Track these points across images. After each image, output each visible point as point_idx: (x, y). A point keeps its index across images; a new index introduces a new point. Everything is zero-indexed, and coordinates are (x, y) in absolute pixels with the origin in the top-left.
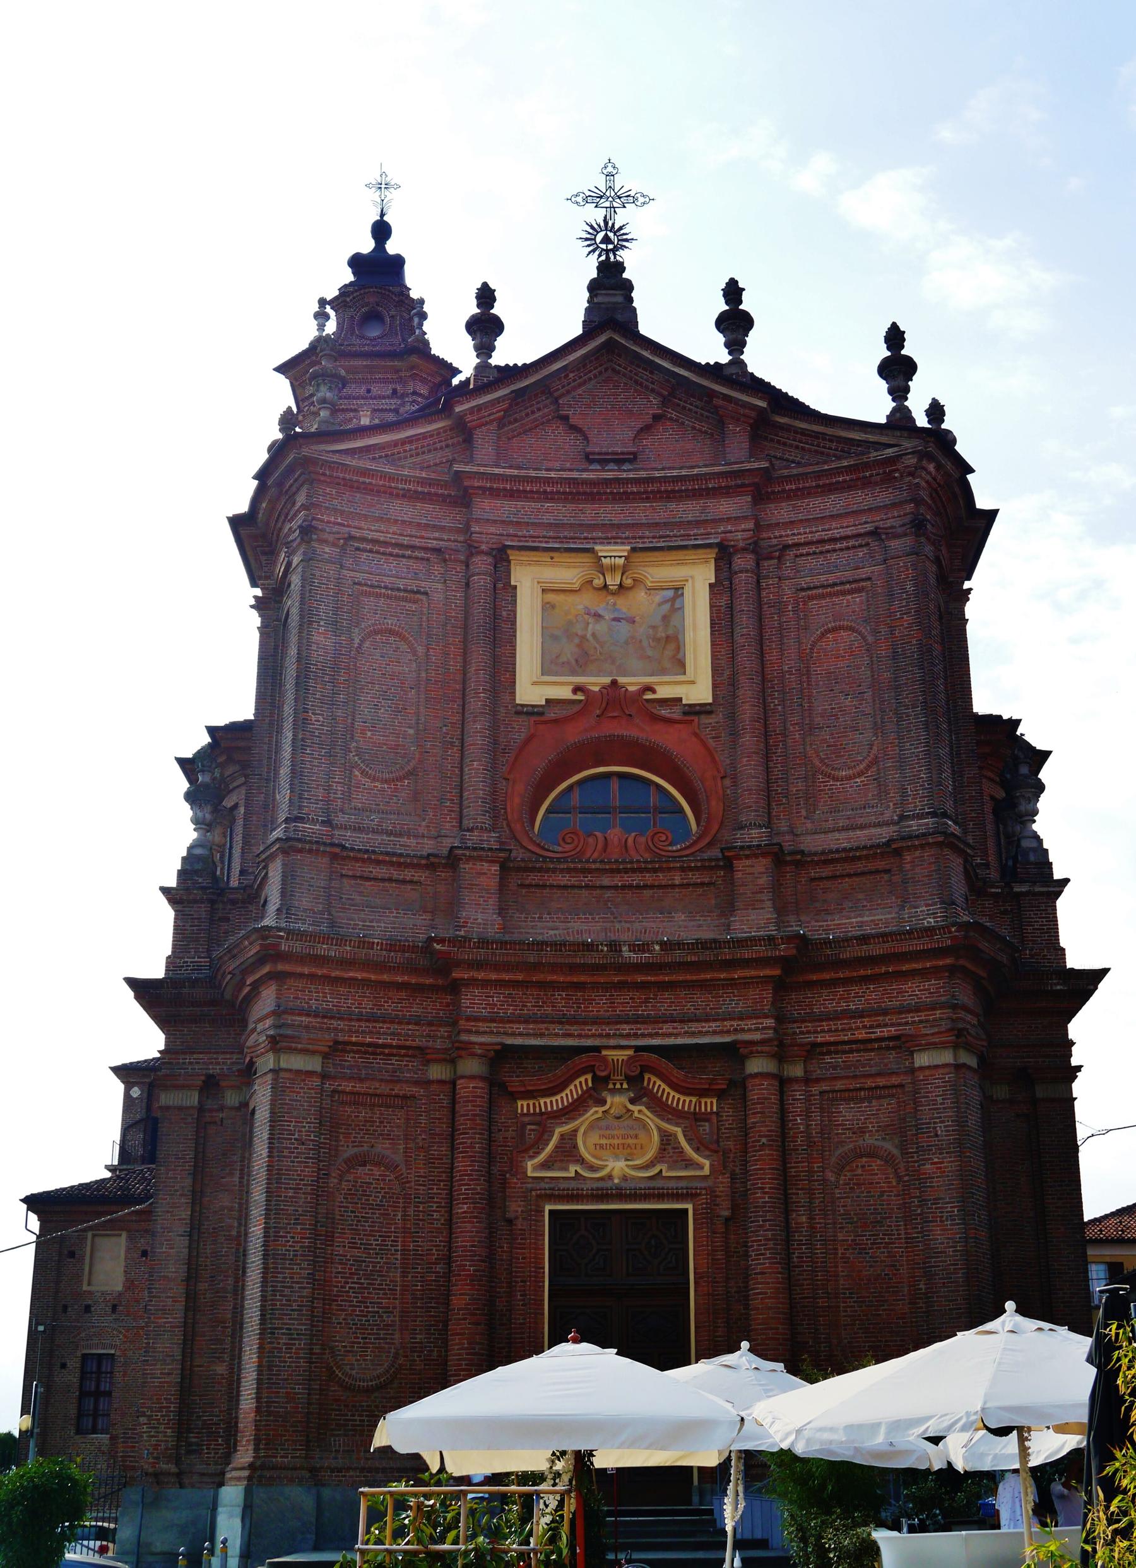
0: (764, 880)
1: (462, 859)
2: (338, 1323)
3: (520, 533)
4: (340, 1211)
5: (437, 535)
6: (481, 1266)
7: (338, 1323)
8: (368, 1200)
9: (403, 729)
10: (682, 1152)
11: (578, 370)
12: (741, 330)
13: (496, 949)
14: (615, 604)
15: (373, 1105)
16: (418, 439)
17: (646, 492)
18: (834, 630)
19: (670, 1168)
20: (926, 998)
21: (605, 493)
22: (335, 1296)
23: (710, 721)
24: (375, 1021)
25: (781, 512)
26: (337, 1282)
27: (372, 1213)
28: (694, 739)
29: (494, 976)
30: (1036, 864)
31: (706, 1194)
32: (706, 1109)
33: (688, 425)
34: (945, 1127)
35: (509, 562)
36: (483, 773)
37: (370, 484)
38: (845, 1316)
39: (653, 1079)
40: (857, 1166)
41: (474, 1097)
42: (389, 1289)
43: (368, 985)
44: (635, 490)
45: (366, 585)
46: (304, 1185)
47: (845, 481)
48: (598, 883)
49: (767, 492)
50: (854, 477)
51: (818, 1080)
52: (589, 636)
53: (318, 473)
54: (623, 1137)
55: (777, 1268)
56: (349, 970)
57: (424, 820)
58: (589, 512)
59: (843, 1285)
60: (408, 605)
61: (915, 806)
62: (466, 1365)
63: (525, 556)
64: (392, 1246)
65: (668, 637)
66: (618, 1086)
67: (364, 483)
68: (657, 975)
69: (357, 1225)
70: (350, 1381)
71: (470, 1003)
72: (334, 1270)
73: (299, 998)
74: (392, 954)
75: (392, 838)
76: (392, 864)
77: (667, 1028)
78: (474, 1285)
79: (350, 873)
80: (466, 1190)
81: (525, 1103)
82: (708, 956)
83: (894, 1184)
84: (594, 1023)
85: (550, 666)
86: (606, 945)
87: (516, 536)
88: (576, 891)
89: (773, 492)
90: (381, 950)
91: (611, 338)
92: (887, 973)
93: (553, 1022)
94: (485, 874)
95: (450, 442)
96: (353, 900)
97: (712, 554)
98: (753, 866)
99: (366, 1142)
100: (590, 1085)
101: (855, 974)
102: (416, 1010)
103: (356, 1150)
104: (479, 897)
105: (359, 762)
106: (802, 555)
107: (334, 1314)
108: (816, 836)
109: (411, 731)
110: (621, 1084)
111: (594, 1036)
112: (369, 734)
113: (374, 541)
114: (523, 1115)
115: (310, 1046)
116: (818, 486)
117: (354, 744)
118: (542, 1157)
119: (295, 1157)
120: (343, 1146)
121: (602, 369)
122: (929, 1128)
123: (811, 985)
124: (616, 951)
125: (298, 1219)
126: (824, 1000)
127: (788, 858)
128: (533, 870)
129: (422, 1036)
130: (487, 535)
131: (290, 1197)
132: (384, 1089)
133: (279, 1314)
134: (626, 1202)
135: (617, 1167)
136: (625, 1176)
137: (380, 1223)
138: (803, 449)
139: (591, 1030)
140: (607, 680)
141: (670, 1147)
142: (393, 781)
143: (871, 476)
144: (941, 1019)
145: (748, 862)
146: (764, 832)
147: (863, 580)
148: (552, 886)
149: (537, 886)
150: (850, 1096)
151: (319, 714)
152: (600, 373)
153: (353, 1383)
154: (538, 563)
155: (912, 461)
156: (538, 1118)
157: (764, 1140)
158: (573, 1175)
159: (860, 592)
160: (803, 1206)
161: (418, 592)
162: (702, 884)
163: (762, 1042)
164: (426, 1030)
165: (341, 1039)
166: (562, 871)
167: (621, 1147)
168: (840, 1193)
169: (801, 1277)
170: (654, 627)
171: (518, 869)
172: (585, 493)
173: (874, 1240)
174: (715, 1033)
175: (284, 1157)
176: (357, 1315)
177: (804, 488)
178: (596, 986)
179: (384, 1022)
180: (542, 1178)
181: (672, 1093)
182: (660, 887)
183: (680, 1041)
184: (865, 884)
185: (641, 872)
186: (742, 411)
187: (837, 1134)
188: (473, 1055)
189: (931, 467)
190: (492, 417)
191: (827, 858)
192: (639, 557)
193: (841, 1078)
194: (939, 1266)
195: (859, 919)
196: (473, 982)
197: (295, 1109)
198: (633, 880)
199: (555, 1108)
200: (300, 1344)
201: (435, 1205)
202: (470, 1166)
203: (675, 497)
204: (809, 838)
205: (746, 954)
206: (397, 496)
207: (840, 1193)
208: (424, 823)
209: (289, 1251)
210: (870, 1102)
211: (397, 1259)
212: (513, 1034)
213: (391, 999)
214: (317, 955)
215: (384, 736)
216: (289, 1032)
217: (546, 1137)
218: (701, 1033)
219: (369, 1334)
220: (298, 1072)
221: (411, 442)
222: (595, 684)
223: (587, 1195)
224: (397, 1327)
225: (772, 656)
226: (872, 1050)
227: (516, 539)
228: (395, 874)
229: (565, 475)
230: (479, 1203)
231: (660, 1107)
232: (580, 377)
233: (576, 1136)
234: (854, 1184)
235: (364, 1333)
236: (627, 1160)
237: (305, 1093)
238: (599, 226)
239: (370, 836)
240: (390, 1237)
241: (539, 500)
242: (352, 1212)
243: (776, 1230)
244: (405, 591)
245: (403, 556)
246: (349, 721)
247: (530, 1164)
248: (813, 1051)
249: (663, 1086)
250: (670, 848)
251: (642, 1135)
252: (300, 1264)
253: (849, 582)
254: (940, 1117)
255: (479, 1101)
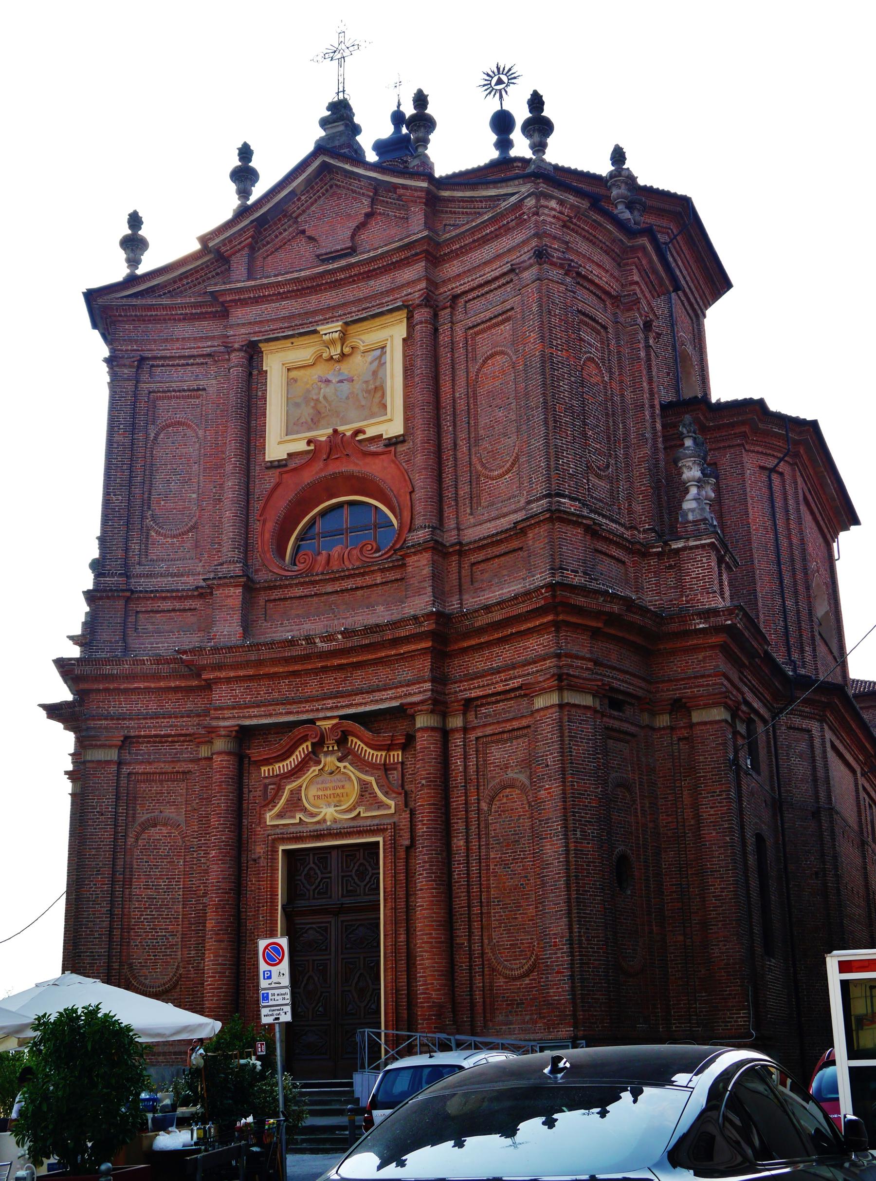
0: (427, 571)
1: (213, 588)
2: (135, 946)
3: (263, 330)
4: (137, 862)
5: (209, 343)
6: (225, 897)
7: (135, 946)
8: (158, 852)
9: (188, 495)
10: (376, 796)
11: (308, 192)
12: (422, 129)
13: (226, 653)
14: (340, 369)
15: (161, 781)
16: (192, 274)
17: (351, 277)
18: (492, 356)
19: (366, 810)
20: (541, 651)
21: (322, 284)
22: (133, 925)
23: (404, 448)
24: (157, 718)
25: (453, 268)
26: (134, 915)
27: (161, 862)
28: (393, 465)
29: (232, 674)
30: (694, 522)
31: (391, 829)
32: (394, 760)
33: (391, 215)
34: (553, 758)
35: (262, 352)
36: (232, 519)
37: (156, 315)
38: (494, 920)
39: (355, 740)
40: (503, 796)
41: (220, 768)
42: (174, 918)
43: (153, 692)
44: (343, 276)
45: (159, 392)
46: (104, 845)
47: (491, 232)
48: (323, 591)
49: (441, 255)
50: (497, 227)
51: (474, 728)
52: (321, 399)
53: (115, 316)
54: (334, 789)
55: (433, 885)
56: (133, 682)
57: (201, 561)
58: (314, 301)
59: (494, 895)
60: (192, 400)
61: (537, 491)
62: (212, 973)
63: (273, 345)
64: (176, 885)
65: (376, 388)
66: (331, 749)
67: (151, 316)
68: (348, 658)
69: (150, 872)
70: (143, 988)
71: (219, 697)
72: (133, 906)
73: (100, 708)
74: (160, 666)
75: (175, 579)
76: (175, 598)
77: (358, 699)
78: (219, 912)
79: (143, 609)
80: (214, 839)
81: (266, 769)
82: (375, 638)
83: (527, 809)
84: (307, 701)
85: (291, 428)
86: (303, 640)
87: (261, 332)
88: (309, 599)
89: (445, 254)
90: (151, 664)
91: (324, 161)
92: (512, 634)
93: (278, 704)
94: (232, 596)
95: (219, 271)
96: (146, 629)
97: (403, 314)
98: (419, 561)
99: (157, 809)
100: (310, 750)
101: (491, 638)
102: (189, 706)
103: (149, 815)
104: (227, 614)
105: (154, 525)
106: (470, 300)
107: (132, 939)
108: (475, 528)
109: (194, 496)
110: (333, 747)
111: (307, 711)
112: (162, 503)
113: (164, 358)
114: (265, 778)
115: (107, 742)
116: (474, 241)
117: (150, 512)
118: (276, 810)
119: (97, 825)
120: (139, 813)
121: (327, 187)
122: (543, 760)
123: (465, 651)
124: (312, 643)
125: (99, 871)
126: (476, 662)
127: (451, 550)
128: (275, 587)
129: (194, 725)
130: (239, 335)
131: (93, 855)
132: (168, 768)
133: (84, 942)
134: (336, 839)
135: (329, 813)
136: (335, 819)
137: (167, 868)
138: (467, 213)
139: (305, 707)
140: (330, 431)
141: (367, 793)
142: (180, 535)
143: (508, 223)
144: (550, 667)
145: (416, 558)
146: (427, 532)
147: (508, 310)
148: (291, 598)
149: (280, 599)
150: (498, 738)
151: (118, 495)
152: (327, 191)
153: (145, 989)
154: (283, 349)
155: (531, 202)
156: (275, 780)
157: (424, 782)
158: (297, 821)
159: (509, 321)
160: (461, 833)
161: (198, 390)
162: (396, 580)
163: (422, 702)
164: (196, 720)
165: (132, 734)
166: (296, 585)
167: (332, 796)
168: (492, 819)
169: (459, 890)
170: (366, 382)
171: (265, 589)
172: (308, 288)
173: (514, 856)
174: (391, 699)
175: (89, 825)
176: (149, 939)
177: (465, 245)
178: (308, 672)
179: (164, 718)
180: (277, 826)
181: (369, 750)
182: (368, 587)
183: (368, 708)
184: (508, 562)
185: (353, 578)
186: (416, 194)
187: (490, 771)
188: (219, 736)
189: (553, 204)
190: (242, 245)
191: (482, 545)
192: (352, 329)
193: (490, 724)
194: (549, 876)
195: (500, 592)
196: (218, 681)
197: (97, 790)
198: (348, 585)
199: (282, 772)
200: (100, 963)
201: (203, 852)
202: (216, 821)
203: (372, 276)
204: (470, 531)
205: (402, 633)
206: (180, 320)
207: (492, 819)
208: (201, 564)
209: (92, 894)
210: (511, 743)
211: (180, 895)
212: (250, 717)
213: (171, 700)
214: (103, 674)
215: (174, 503)
216: (93, 733)
217: (280, 794)
218: (382, 700)
219: (158, 952)
220: (99, 762)
221: (186, 277)
222: (322, 435)
223: (307, 836)
224: (180, 946)
225: (446, 387)
226: (511, 699)
227: (261, 334)
228: (178, 605)
229: (289, 277)
230: (223, 849)
231: (361, 763)
232: (311, 198)
233: (301, 790)
234: (501, 811)
235: (155, 952)
236: (336, 806)
237: (104, 777)
238: (493, 72)
239: (159, 580)
240: (175, 878)
241: (277, 301)
242: (146, 862)
243: (432, 854)
244: (189, 390)
245: (188, 364)
246: (146, 496)
247: (268, 815)
248: (468, 704)
249: (362, 745)
250: (375, 555)
251: (348, 785)
252: (100, 904)
253: (500, 315)
254: (550, 750)
255: (224, 771)
